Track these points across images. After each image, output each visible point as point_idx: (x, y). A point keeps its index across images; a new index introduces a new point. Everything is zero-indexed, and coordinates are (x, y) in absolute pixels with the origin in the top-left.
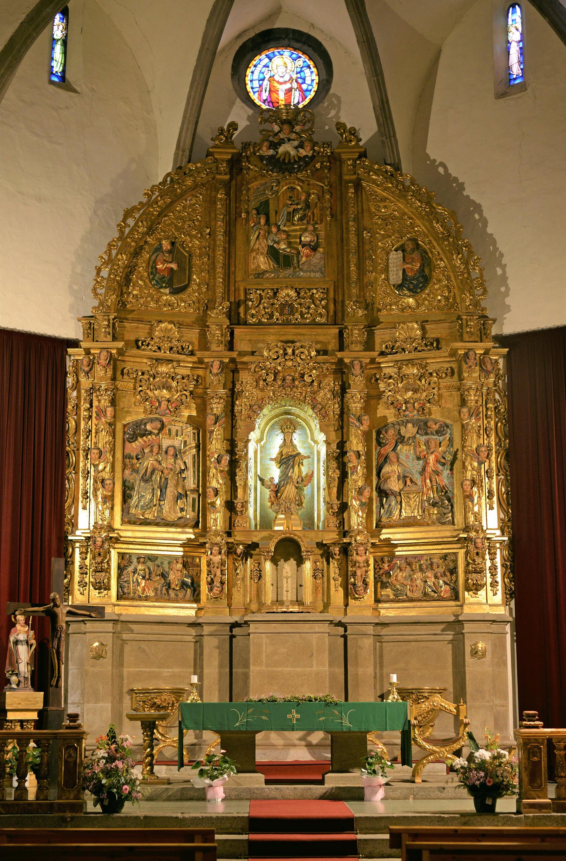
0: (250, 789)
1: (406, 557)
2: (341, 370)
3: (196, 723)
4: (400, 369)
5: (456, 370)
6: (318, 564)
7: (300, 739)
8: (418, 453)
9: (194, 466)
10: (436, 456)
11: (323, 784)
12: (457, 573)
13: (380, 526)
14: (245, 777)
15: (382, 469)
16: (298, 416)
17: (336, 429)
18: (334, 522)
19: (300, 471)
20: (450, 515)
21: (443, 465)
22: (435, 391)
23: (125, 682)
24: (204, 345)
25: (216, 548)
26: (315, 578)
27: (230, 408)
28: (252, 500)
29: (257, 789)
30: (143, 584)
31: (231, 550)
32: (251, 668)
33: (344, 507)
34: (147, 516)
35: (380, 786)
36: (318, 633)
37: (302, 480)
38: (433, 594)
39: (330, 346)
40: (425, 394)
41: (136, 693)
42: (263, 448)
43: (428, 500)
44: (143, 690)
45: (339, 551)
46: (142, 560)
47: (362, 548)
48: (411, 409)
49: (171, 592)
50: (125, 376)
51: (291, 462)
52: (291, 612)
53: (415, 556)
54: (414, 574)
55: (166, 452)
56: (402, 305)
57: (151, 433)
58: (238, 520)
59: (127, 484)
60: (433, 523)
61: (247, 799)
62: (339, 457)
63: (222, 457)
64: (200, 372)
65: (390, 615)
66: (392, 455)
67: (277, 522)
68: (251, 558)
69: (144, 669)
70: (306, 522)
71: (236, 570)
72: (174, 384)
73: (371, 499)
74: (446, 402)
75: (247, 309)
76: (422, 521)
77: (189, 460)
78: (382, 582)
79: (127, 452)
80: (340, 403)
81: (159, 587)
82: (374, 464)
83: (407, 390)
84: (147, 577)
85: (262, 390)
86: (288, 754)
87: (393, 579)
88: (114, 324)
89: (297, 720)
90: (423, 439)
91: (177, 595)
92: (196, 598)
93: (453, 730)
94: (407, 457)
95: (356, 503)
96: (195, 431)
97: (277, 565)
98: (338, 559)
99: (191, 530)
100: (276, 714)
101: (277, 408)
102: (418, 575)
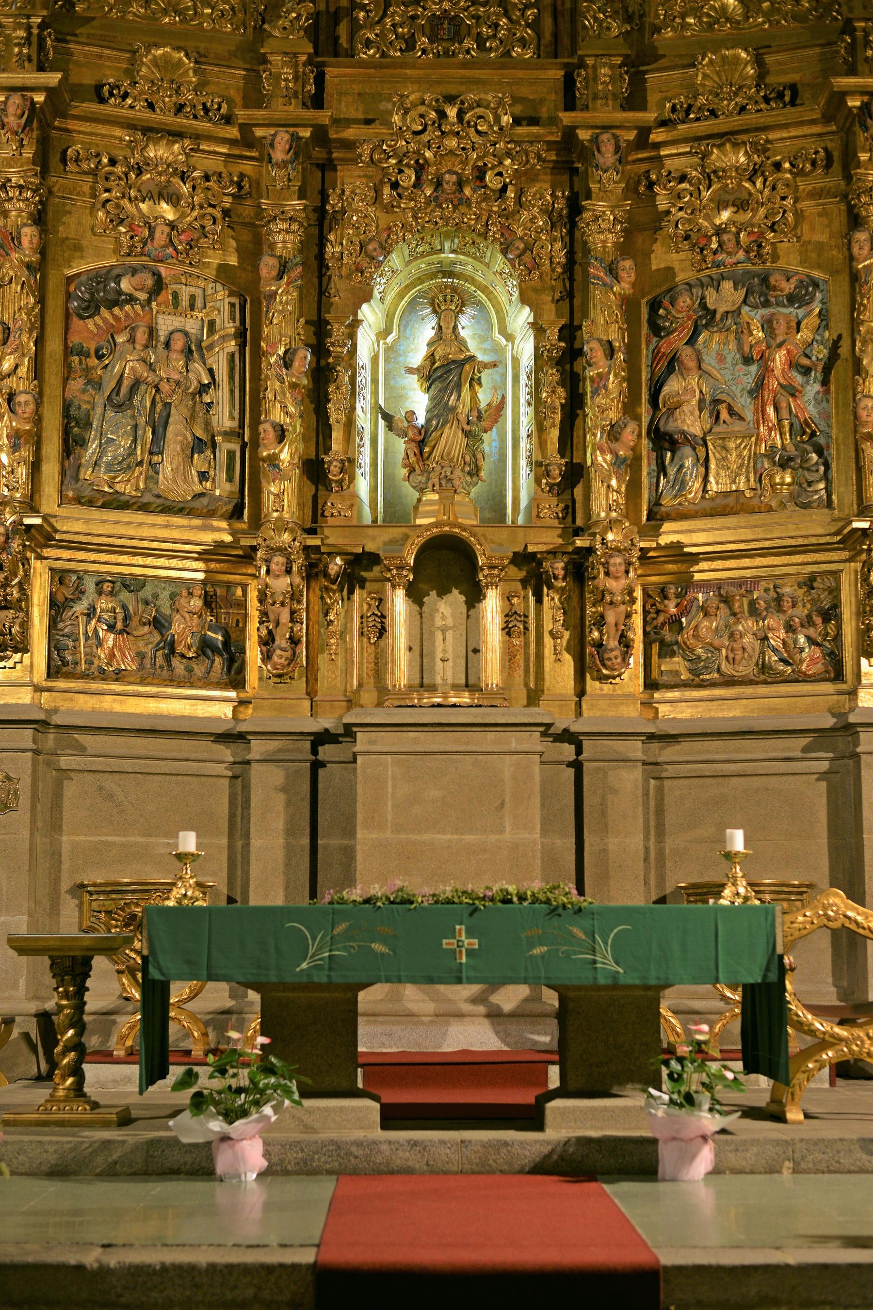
0: (337, 1145)
1: (718, 585)
2: (570, 162)
3: (189, 963)
4: (705, 156)
5: (836, 154)
6: (515, 601)
7: (474, 1001)
8: (747, 349)
9: (231, 378)
10: (789, 352)
11: (539, 1126)
12: (839, 619)
13: (657, 517)
14: (326, 1109)
15: (661, 386)
16: (472, 281)
17: (558, 295)
18: (551, 506)
19: (474, 399)
20: (822, 485)
21: (806, 371)
22: (789, 202)
23: (65, 866)
24: (254, 96)
25: (278, 561)
26: (509, 634)
27: (315, 250)
28: (365, 460)
29: (359, 1144)
30: (110, 642)
31: (314, 570)
32: (359, 835)
33: (575, 474)
34: (119, 487)
35: (704, 1138)
36: (517, 753)
37: (479, 418)
38: (781, 667)
39: (544, 109)
40: (762, 211)
41: (91, 893)
42: (389, 345)
43: (770, 454)
44: (106, 884)
45: (565, 569)
46: (107, 587)
47: (618, 560)
48: (730, 246)
49: (176, 662)
50: (71, 167)
51: (453, 377)
52: (454, 706)
53: (739, 583)
54: (738, 621)
55: (167, 345)
56: (708, 15)
57: (131, 299)
58: (334, 503)
59: (73, 412)
60: (783, 505)
61: (330, 1172)
62: (565, 359)
63: (295, 351)
64: (247, 167)
65: (679, 716)
66: (687, 354)
67: (421, 509)
68: (362, 587)
69: (110, 839)
70: (488, 515)
71: (326, 614)
72: (185, 189)
73: (637, 458)
74: (812, 229)
75: (355, 27)
76: (756, 501)
77: (220, 364)
78: (662, 643)
79: (75, 340)
80: (567, 239)
81: (149, 650)
82: (645, 376)
83: (721, 205)
84: (119, 625)
85: (389, 209)
86: (444, 1034)
87: (687, 636)
88: (41, 41)
89: (470, 953)
90: (754, 317)
91: (190, 670)
92: (236, 680)
93: (830, 980)
94: (721, 359)
95: (603, 460)
96: (235, 300)
97: (421, 604)
98: (563, 589)
99: (224, 524)
100: (414, 937)
101: (423, 255)
102: (747, 625)
